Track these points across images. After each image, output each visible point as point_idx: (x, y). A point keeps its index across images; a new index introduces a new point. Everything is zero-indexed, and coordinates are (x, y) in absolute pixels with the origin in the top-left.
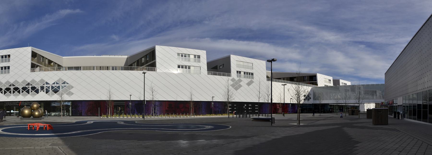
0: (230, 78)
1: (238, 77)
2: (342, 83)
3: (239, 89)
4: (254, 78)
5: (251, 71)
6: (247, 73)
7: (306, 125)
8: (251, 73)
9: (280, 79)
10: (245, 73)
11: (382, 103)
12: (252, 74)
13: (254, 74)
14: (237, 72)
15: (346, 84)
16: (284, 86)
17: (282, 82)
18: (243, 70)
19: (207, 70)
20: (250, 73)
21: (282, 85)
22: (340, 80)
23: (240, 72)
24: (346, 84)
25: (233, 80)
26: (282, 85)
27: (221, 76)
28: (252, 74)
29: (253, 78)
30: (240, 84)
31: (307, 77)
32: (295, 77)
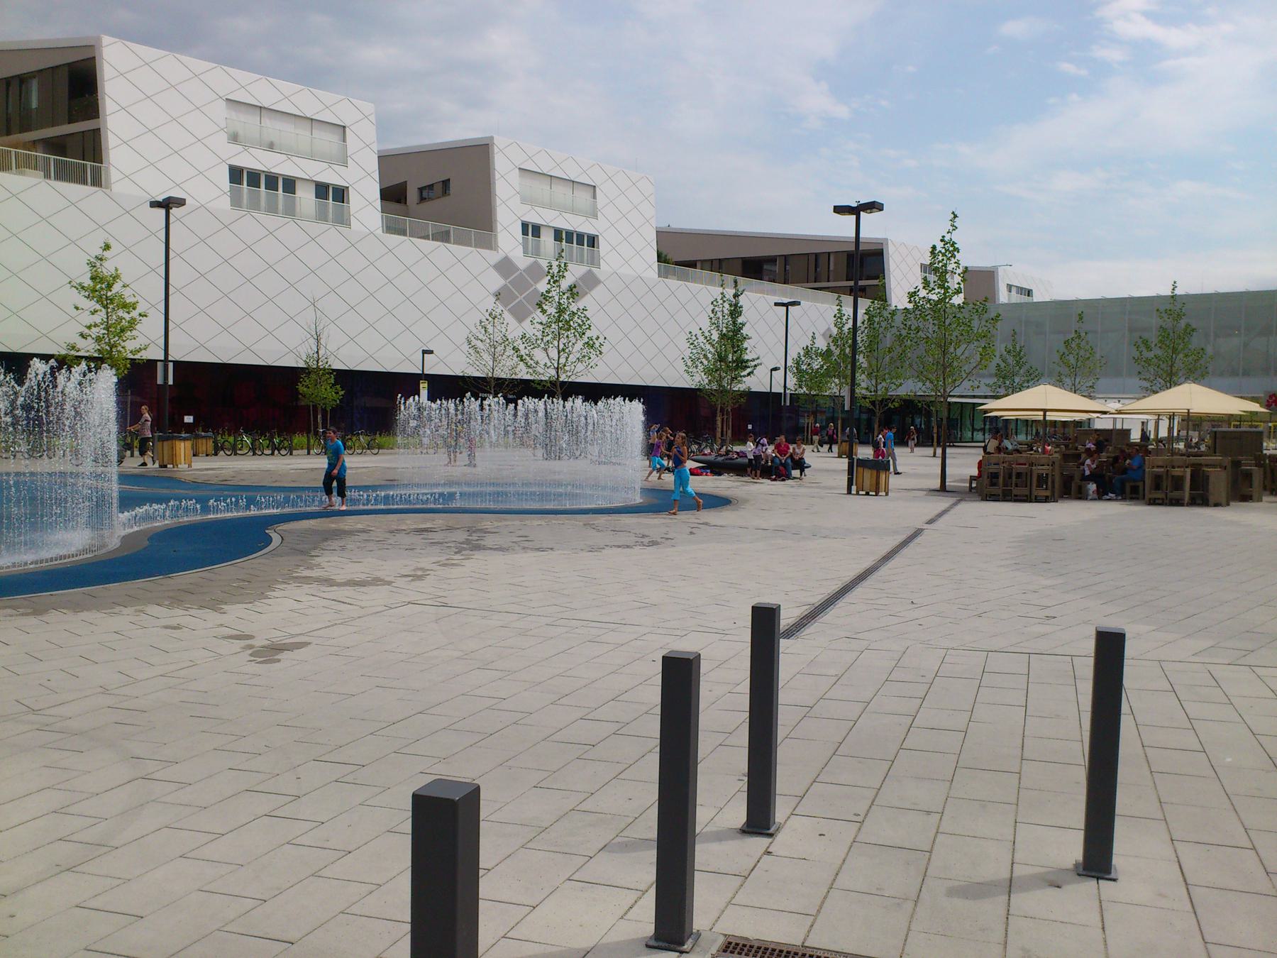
0: (494, 257)
1: (525, 252)
2: (1010, 287)
3: (587, 293)
4: (353, 220)
5: (586, 228)
6: (570, 235)
7: (852, 367)
8: (589, 236)
9: (692, 264)
10: (558, 234)
11: (1271, 397)
12: (593, 241)
13: (601, 242)
14: (525, 226)
15: (1029, 293)
16: (163, 211)
17: (774, 293)
18: (551, 218)
19: (380, 209)
20: (580, 237)
21: (776, 304)
22: (106, 40)
23: (537, 230)
24: (1029, 293)
25: (505, 266)
26: (776, 304)
27: (429, 239)
28: (593, 241)
29: (594, 261)
30: (505, 276)
31: (34, 86)
32: (772, 260)
